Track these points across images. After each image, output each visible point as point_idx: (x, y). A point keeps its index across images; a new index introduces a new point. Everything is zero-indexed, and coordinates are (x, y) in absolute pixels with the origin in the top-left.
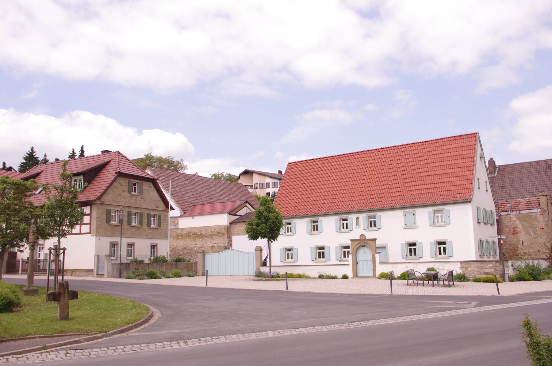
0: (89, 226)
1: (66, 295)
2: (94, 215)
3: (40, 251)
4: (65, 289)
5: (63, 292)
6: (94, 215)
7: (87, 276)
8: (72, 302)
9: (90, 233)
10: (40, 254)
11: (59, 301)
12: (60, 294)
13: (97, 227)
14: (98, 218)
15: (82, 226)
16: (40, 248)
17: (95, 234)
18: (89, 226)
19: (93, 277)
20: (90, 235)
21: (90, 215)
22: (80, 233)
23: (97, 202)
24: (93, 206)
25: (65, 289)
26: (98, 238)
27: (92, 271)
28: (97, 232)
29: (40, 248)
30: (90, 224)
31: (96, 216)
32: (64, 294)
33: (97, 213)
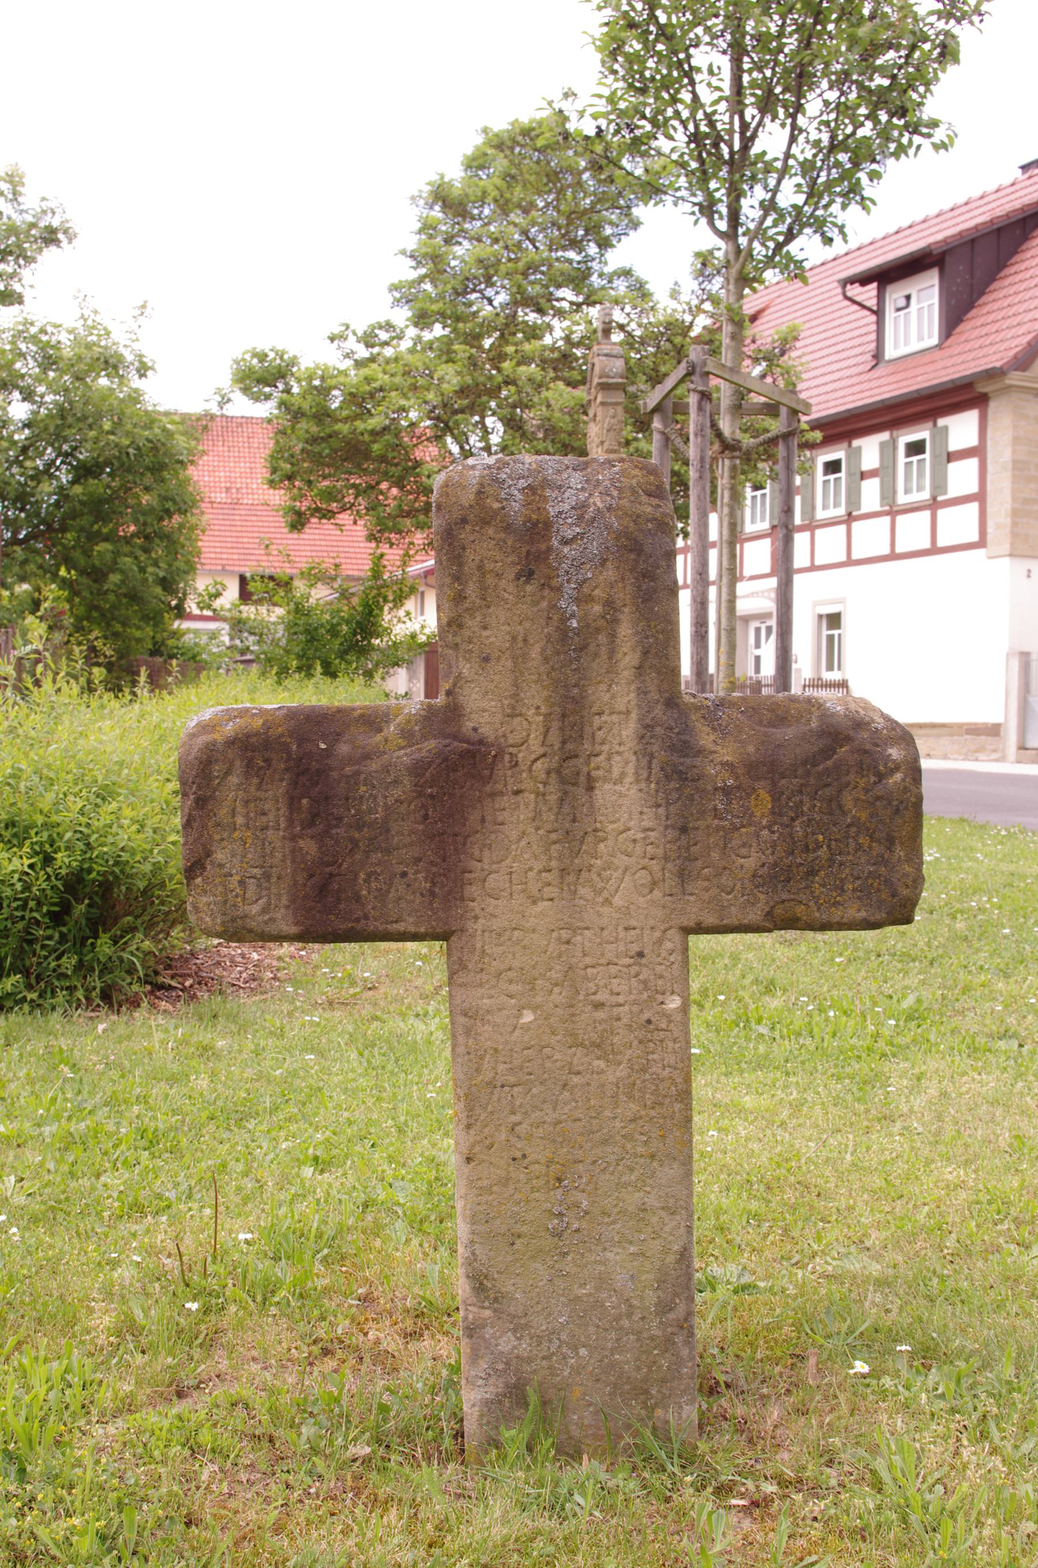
0: (975, 506)
1: (625, 801)
2: (1001, 451)
3: (758, 645)
4: (573, 650)
5: (529, 736)
6: (1001, 451)
7: (972, 755)
8: (759, 981)
9: (981, 543)
10: (758, 659)
11: (442, 923)
12: (458, 770)
13: (1015, 513)
14: (1018, 466)
15: (941, 513)
16: (758, 630)
17: (1006, 548)
18: (975, 506)
19: (1002, 759)
20: (981, 552)
21: (977, 452)
22: (934, 550)
23: (1014, 378)
24: (992, 405)
25: (573, 650)
26: (1023, 565)
27: (994, 730)
28: (1014, 535)
29: (758, 630)
30: (980, 497)
31: (1007, 455)
32: (572, 776)
33: (1016, 440)
